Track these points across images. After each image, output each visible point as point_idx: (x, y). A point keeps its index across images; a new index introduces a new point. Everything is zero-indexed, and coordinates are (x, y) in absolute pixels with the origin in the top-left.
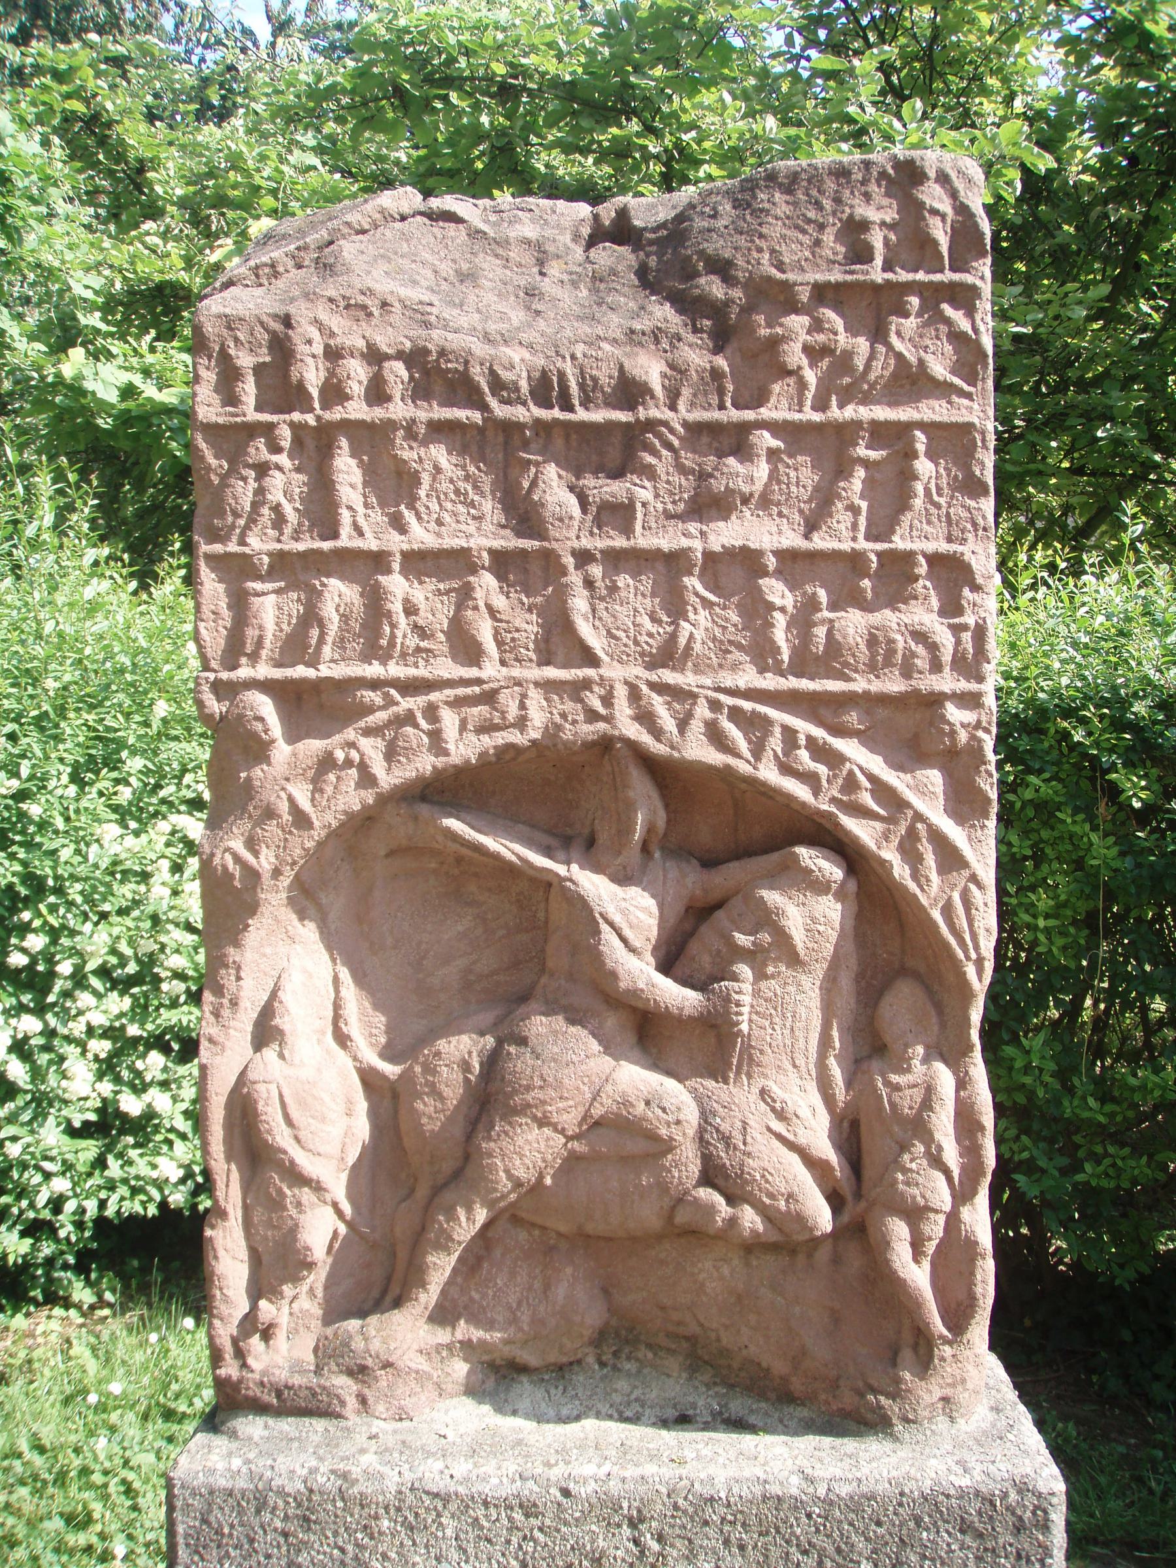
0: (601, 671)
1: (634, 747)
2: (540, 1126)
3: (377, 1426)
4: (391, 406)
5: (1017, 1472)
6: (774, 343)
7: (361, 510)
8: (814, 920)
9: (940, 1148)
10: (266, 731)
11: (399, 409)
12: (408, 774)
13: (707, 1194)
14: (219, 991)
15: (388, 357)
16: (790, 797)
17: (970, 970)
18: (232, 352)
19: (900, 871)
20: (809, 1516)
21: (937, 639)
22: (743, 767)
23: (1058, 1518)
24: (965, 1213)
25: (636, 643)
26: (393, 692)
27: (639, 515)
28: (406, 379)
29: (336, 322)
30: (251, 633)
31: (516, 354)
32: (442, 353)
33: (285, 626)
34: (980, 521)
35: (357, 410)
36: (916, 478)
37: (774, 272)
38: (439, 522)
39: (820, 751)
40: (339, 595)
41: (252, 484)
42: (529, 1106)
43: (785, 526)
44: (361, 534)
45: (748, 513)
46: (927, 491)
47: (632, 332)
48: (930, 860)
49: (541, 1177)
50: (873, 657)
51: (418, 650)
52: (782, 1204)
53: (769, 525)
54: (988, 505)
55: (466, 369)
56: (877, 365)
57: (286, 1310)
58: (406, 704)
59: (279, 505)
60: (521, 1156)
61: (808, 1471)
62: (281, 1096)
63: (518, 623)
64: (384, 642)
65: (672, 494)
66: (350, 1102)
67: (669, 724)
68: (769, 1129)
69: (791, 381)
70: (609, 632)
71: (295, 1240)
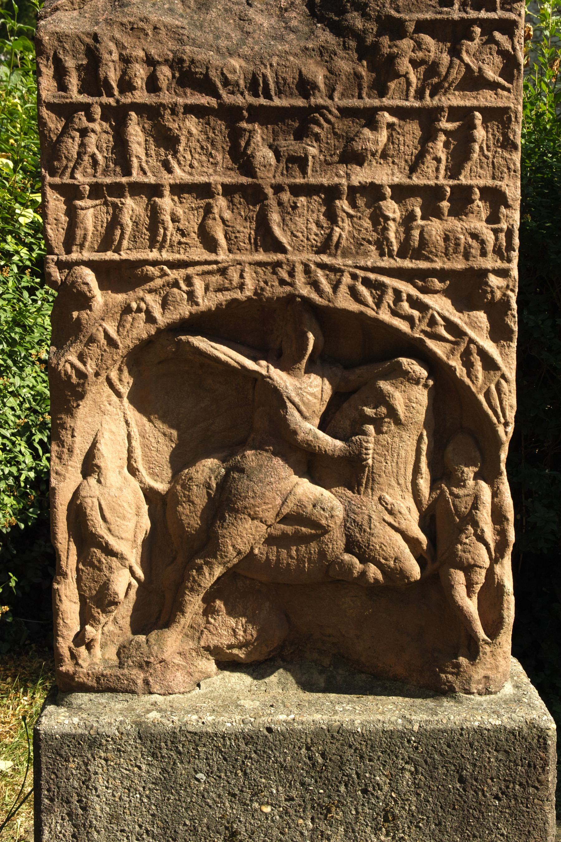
0: (288, 256)
1: (306, 301)
2: (253, 519)
3: (155, 698)
4: (161, 94)
5: (528, 718)
6: (392, 58)
7: (144, 158)
8: (410, 400)
9: (483, 531)
10: (90, 292)
11: (166, 98)
12: (174, 317)
13: (347, 557)
14: (61, 443)
15: (159, 63)
16: (397, 331)
17: (501, 429)
18: (61, 57)
19: (461, 371)
20: (409, 741)
21: (485, 238)
22: (370, 313)
23: (552, 742)
24: (498, 569)
25: (308, 239)
26: (165, 268)
27: (310, 164)
28: (170, 77)
29: (126, 40)
30: (79, 233)
31: (236, 63)
32: (192, 61)
33: (99, 228)
34: (512, 166)
35: (140, 96)
36: (475, 141)
37: (393, 12)
38: (191, 166)
39: (415, 303)
40: (132, 207)
41: (78, 140)
42: (246, 508)
43: (396, 171)
44: (145, 173)
45: (374, 163)
46: (481, 148)
47: (307, 49)
48: (478, 365)
49: (252, 549)
50: (446, 249)
51: (180, 243)
52: (392, 563)
53: (387, 170)
54: (517, 157)
55: (207, 72)
56: (454, 71)
57: (100, 631)
58: (173, 274)
59: (94, 154)
60: (242, 537)
61: (408, 716)
62: (100, 505)
63: (238, 227)
64: (160, 239)
65: (329, 150)
66: (138, 508)
67: (326, 287)
68: (384, 520)
69: (402, 80)
70: (292, 233)
71: (108, 589)
